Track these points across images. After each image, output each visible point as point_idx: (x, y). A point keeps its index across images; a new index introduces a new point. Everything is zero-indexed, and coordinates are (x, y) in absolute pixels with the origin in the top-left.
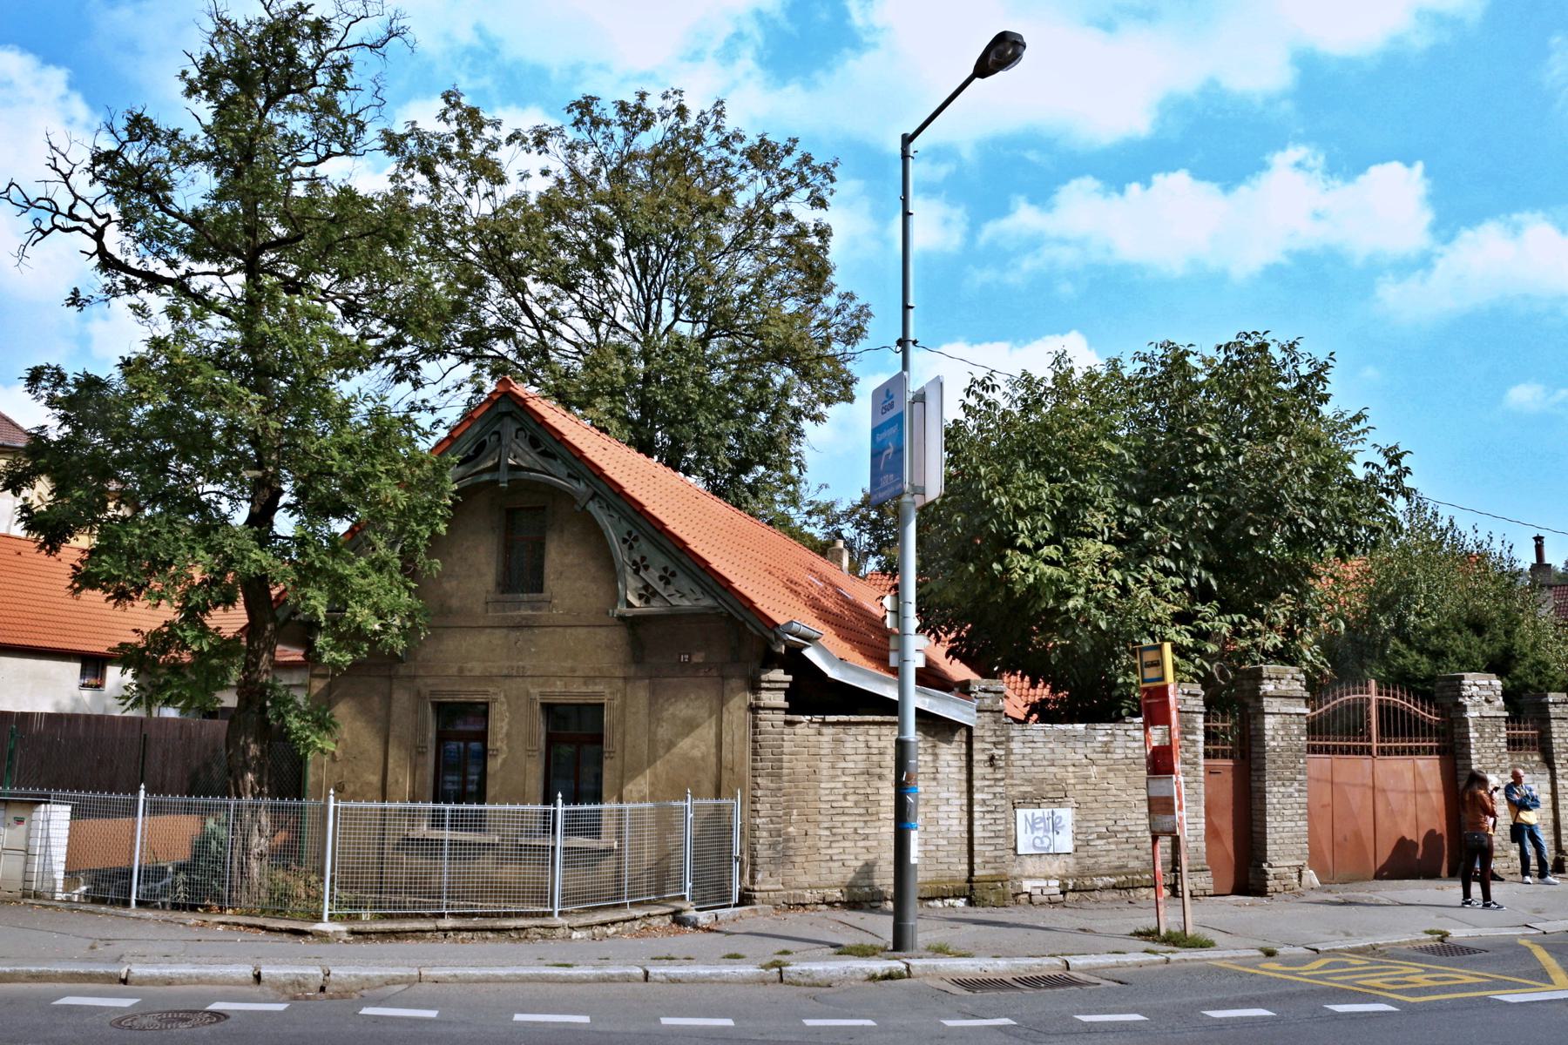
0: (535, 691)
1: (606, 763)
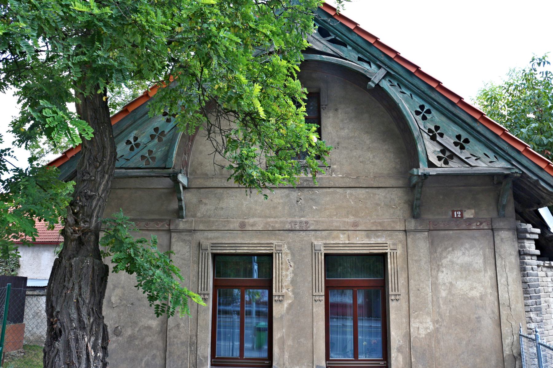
0: (319, 243)
1: (392, 305)
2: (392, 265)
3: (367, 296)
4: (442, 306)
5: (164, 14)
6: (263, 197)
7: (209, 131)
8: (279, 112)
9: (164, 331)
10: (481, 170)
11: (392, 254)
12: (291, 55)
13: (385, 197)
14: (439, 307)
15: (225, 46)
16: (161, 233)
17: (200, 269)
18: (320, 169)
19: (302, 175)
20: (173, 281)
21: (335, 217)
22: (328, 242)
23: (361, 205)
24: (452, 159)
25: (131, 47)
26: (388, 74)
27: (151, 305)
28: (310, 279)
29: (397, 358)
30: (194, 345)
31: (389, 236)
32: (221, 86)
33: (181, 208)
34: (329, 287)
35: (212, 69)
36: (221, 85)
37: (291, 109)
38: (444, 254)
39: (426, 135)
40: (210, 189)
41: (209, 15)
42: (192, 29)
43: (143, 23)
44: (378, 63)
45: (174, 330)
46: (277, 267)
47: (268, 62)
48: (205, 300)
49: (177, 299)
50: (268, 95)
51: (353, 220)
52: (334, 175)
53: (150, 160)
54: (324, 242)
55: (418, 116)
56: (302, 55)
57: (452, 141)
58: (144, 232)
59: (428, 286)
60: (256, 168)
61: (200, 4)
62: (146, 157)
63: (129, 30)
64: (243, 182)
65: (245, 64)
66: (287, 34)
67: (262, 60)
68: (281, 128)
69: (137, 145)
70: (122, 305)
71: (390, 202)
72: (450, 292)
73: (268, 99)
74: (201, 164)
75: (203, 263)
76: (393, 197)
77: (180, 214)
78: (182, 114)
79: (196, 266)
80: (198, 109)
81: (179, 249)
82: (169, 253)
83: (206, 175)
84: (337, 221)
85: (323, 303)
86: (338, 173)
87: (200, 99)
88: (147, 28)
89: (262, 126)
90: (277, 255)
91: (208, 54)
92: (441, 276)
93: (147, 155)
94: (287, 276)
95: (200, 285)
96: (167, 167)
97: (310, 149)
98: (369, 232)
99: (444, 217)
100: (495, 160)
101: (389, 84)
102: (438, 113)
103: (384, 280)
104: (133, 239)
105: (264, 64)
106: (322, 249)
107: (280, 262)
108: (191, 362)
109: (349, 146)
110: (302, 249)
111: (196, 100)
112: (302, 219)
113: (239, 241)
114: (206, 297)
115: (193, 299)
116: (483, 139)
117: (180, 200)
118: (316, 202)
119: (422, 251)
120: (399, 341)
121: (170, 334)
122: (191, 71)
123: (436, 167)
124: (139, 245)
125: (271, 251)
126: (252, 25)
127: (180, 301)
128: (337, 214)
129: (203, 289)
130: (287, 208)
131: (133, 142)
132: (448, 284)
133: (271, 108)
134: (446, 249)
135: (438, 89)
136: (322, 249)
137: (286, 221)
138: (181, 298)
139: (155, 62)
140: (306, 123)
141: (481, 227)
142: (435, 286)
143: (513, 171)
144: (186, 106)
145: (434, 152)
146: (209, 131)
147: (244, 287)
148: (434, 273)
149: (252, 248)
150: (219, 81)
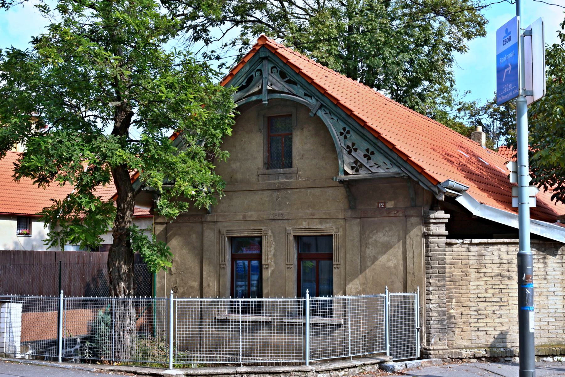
0: (289, 228)
10: (379, 175)
39: (345, 151)
54: (293, 227)
57: (363, 154)
94: (270, 251)
100: (391, 166)
106: (292, 232)
113: (242, 228)
116: (382, 151)
123: (349, 174)
134: (372, 231)
136: (292, 232)
141: (398, 215)
143: (402, 175)
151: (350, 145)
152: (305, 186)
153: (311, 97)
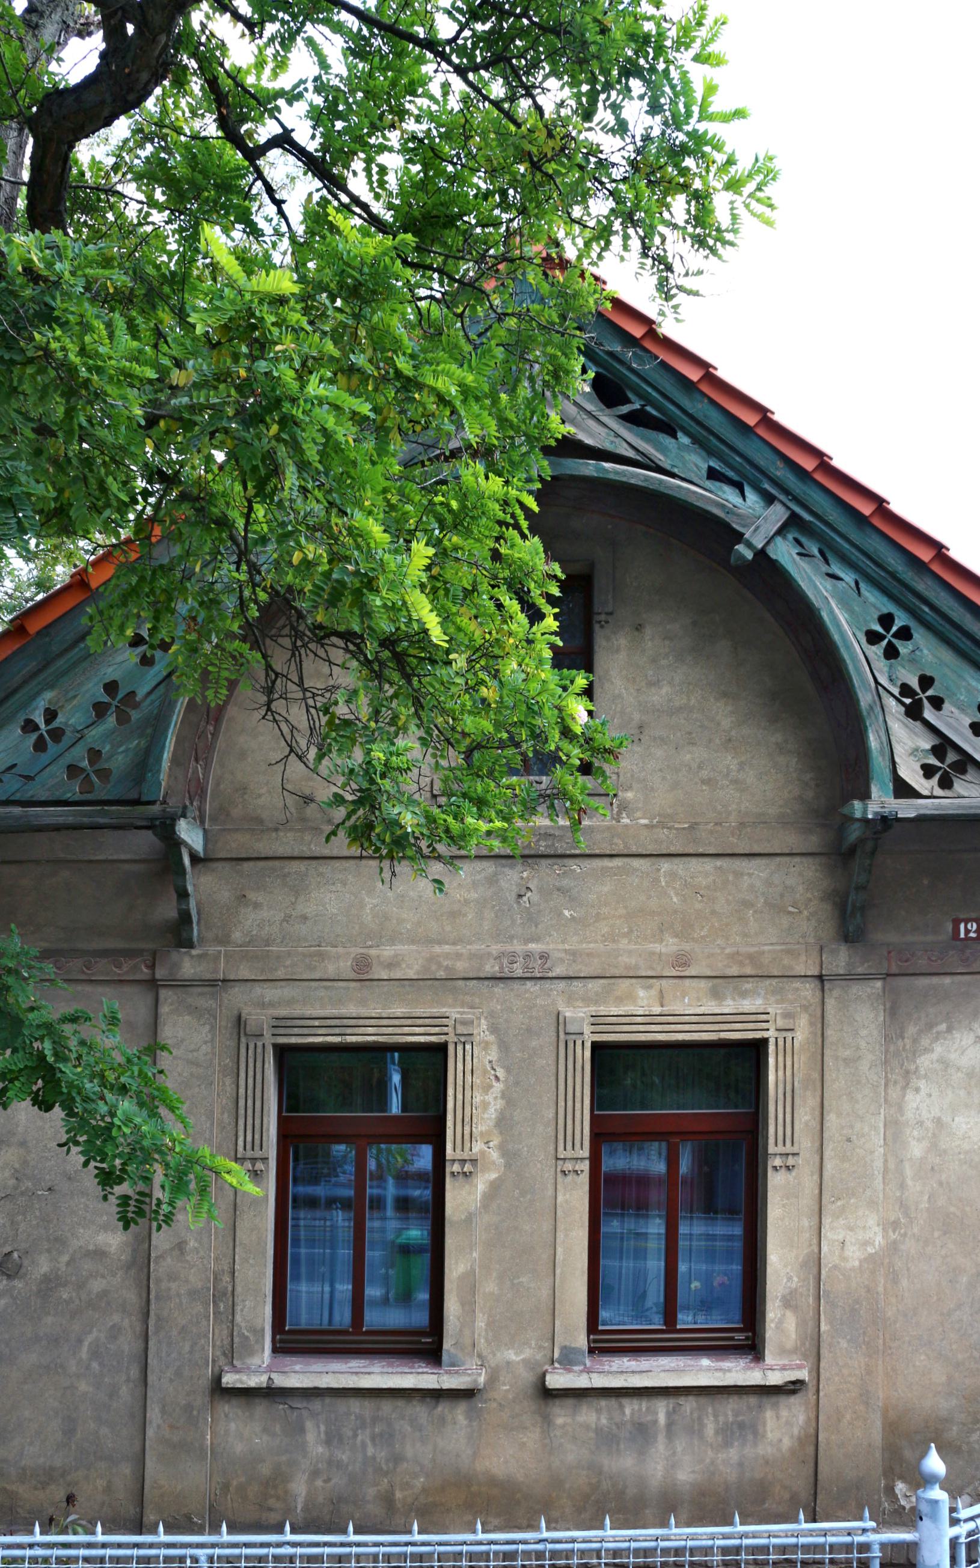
0: (578, 1015)
1: (776, 1183)
2: (781, 1073)
3: (706, 1160)
4: (909, 1182)
5: (133, 330)
6: (431, 887)
7: (269, 690)
8: (478, 634)
9: (142, 1263)
11: (781, 1043)
12: (512, 463)
13: (768, 883)
14: (902, 1186)
15: (324, 431)
16: (128, 989)
17: (242, 1091)
18: (593, 802)
19: (541, 821)
20: (167, 1128)
21: (625, 941)
22: (603, 1010)
23: (698, 906)
24: (964, 772)
25: (32, 436)
26: (793, 522)
27: (105, 1198)
28: (551, 1114)
29: (781, 1322)
30: (224, 1296)
31: (774, 993)
32: (311, 556)
33: (185, 918)
34: (602, 1135)
35: (280, 504)
36: (311, 550)
37: (514, 627)
38: (925, 1042)
39: (892, 702)
40: (270, 863)
41: (275, 331)
42: (223, 377)
43: (72, 357)
44: (767, 486)
45: (169, 1260)
46: (460, 1082)
47: (443, 482)
48: (256, 1175)
49: (180, 1179)
50: (445, 583)
51: (675, 948)
52: (626, 821)
53: (94, 778)
54: (593, 1009)
55: (874, 648)
56: (545, 463)
57: (967, 721)
58: (79, 988)
59: (876, 1128)
60: (411, 802)
61: (248, 297)
62: (83, 770)
63: (28, 380)
64: (371, 844)
65: (379, 488)
66: (503, 396)
67: (425, 476)
68: (482, 682)
69: (57, 735)
70: (22, 1194)
71: (782, 896)
72: (934, 1146)
73: (446, 595)
74: (244, 789)
75: (251, 1073)
76: (791, 881)
77: (185, 935)
78: (187, 643)
79: (228, 1081)
80: (235, 627)
81: (180, 1034)
82: (153, 1048)
83: (260, 821)
84: (630, 952)
85: (585, 1179)
86: (638, 814)
87: (241, 598)
88: (83, 372)
89: (428, 679)
90: (460, 1048)
91: (270, 456)
92: (912, 1101)
93: (85, 763)
94: (485, 1105)
95: (241, 1133)
96: (144, 798)
97: (566, 745)
98: (721, 982)
99: (930, 938)
101: (794, 551)
102: (930, 637)
103: (757, 1113)
104: (52, 1012)
105: (431, 490)
106: (587, 1030)
107: (469, 1067)
108: (218, 1343)
109: (671, 737)
110: (529, 1030)
111: (230, 603)
112: (532, 946)
113: (352, 1010)
114: (259, 1166)
115: (227, 1177)
117: (183, 895)
118: (572, 899)
119: (864, 1032)
120: (790, 1279)
121: (158, 1270)
122: (214, 510)
123: (917, 795)
124: (68, 1029)
125: (443, 1038)
126: (404, 365)
127: (187, 1183)
128: (631, 931)
129: (249, 1146)
130: (489, 915)
131: (42, 726)
132: (929, 1124)
133: (454, 623)
134: (930, 1026)
135: (936, 568)
137: (485, 950)
138: (192, 1176)
139: (110, 479)
140: (554, 666)
142: (894, 1129)
144: (199, 619)
145: (914, 752)
146: (269, 690)
147: (362, 1138)
148: (894, 1093)
149: (390, 1030)
150: (303, 540)
151: (914, 683)
152: (651, 849)
153: (740, 488)
